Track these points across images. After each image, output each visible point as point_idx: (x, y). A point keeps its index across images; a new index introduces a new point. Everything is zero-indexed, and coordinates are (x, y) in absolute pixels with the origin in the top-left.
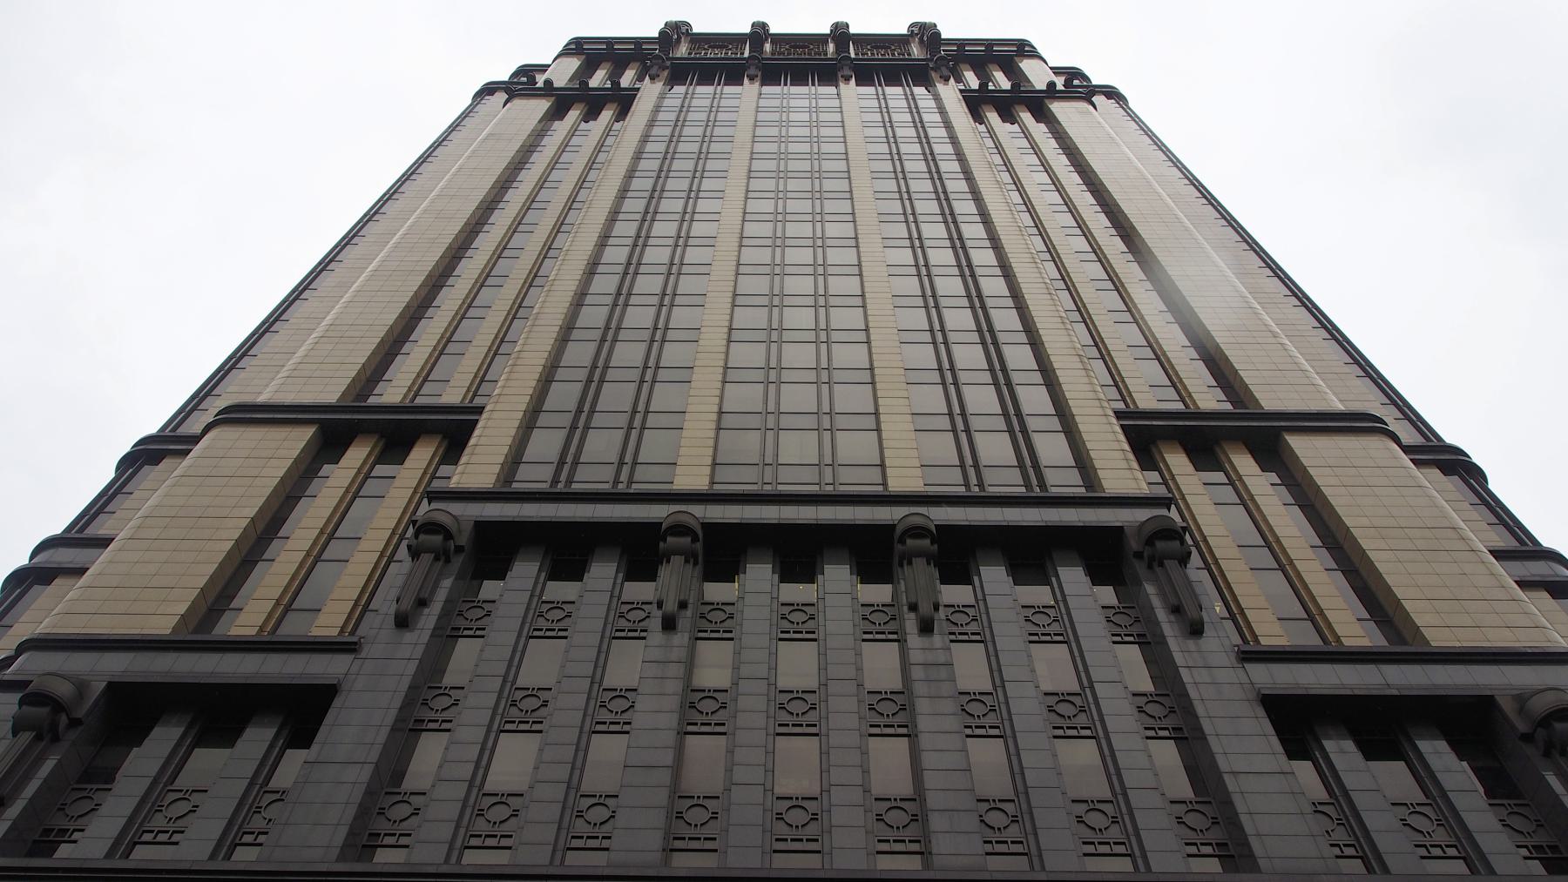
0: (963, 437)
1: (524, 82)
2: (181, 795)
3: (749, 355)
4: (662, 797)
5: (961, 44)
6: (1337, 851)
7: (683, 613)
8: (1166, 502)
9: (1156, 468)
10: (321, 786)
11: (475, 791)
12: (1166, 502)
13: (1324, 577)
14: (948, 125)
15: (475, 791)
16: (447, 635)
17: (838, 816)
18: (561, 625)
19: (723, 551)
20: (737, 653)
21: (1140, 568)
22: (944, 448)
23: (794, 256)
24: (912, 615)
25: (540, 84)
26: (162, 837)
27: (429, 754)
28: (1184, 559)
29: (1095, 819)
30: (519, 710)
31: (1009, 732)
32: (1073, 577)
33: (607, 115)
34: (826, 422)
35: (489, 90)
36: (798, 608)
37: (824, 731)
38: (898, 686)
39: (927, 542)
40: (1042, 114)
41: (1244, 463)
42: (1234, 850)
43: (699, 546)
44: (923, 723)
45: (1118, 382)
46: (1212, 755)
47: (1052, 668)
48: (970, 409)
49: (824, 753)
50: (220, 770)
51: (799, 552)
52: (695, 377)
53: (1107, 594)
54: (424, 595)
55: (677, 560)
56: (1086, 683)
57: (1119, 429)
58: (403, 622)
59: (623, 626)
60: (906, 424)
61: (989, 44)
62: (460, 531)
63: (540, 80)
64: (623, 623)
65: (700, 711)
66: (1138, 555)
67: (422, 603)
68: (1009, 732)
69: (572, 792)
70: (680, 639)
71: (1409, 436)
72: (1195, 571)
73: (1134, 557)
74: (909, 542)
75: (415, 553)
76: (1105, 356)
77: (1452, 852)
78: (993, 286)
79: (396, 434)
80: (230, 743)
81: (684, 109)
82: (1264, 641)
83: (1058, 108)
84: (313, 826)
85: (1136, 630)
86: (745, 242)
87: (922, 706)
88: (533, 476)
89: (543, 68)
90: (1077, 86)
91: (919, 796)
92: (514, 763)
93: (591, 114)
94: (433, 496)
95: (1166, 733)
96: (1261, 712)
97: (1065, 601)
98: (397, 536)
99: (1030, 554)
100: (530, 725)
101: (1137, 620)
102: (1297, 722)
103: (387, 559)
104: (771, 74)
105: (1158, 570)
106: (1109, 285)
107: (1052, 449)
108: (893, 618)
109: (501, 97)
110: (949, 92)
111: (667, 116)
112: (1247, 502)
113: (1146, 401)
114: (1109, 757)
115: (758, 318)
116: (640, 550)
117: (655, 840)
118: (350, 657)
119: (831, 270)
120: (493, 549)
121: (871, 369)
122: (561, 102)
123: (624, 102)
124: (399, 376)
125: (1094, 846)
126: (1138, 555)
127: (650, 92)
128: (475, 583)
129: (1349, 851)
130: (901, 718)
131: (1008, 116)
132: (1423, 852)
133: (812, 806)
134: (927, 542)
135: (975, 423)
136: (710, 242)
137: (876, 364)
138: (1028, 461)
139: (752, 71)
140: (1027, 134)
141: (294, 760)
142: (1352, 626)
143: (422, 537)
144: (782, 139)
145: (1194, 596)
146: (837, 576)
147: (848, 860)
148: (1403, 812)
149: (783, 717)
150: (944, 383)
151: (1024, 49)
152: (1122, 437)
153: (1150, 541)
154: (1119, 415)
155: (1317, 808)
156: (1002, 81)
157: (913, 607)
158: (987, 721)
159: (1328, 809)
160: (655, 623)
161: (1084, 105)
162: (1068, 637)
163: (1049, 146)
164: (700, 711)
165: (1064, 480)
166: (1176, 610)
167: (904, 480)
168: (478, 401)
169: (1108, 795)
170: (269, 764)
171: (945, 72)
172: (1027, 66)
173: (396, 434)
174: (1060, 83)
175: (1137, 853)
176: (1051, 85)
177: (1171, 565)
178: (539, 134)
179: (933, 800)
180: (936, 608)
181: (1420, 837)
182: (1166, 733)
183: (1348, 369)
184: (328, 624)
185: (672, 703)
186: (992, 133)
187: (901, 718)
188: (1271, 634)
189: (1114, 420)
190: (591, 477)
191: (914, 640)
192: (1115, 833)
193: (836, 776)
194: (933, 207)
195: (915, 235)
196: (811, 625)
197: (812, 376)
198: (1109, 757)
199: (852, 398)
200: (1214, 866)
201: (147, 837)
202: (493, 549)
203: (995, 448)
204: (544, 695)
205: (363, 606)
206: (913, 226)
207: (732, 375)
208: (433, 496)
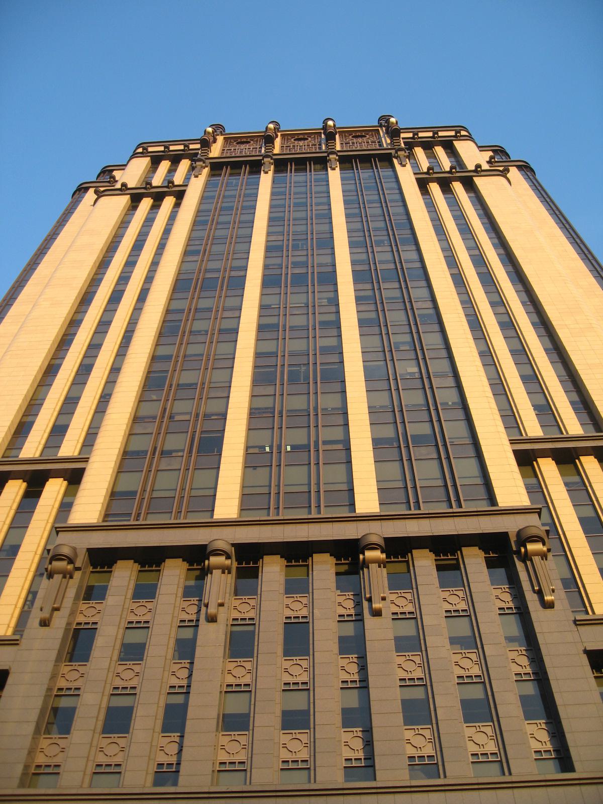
82: (529, 435)
176: (478, 166)
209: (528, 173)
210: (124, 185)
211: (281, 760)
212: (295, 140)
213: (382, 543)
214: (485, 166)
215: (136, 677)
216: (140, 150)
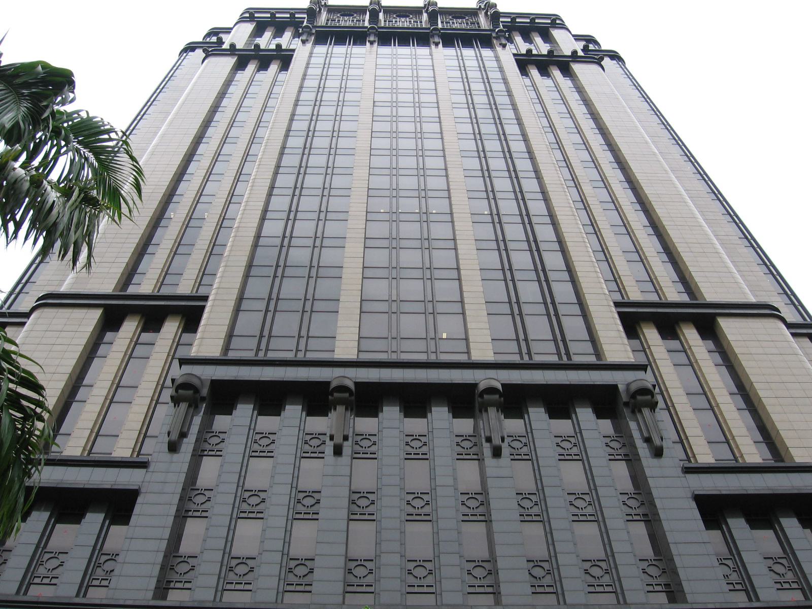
0: (518, 319)
1: (212, 45)
2: (52, 555)
3: (382, 205)
4: (341, 561)
5: (514, 16)
6: (731, 587)
7: (346, 443)
8: (643, 368)
9: (638, 337)
10: (137, 547)
11: (227, 556)
12: (643, 368)
13: (736, 414)
14: (505, 81)
15: (227, 556)
17: (445, 571)
18: (269, 448)
19: (367, 399)
21: (626, 412)
22: (506, 328)
23: (404, 144)
24: (488, 445)
25: (226, 46)
26: (46, 581)
27: (193, 528)
28: (653, 406)
29: (596, 572)
30: (249, 504)
31: (546, 519)
32: (585, 414)
33: (274, 67)
34: (430, 308)
35: (190, 48)
37: (435, 519)
38: (479, 490)
39: (497, 397)
40: (566, 70)
41: (691, 334)
42: (674, 592)
43: (353, 398)
45: (616, 279)
47: (573, 475)
48: (508, 238)
49: (436, 533)
50: (77, 537)
51: (416, 400)
52: (355, 171)
53: (606, 425)
54: (185, 430)
56: (609, 553)
57: (616, 316)
58: (173, 447)
59: (309, 448)
60: (477, 275)
61: (533, 17)
63: (227, 40)
64: (307, 448)
65: (360, 505)
66: (626, 404)
67: (183, 435)
68: (546, 519)
71: (792, 316)
72: (662, 415)
73: (620, 403)
75: (176, 400)
76: (569, 166)
77: (795, 586)
78: (517, 146)
79: (152, 315)
80: (78, 522)
81: (326, 66)
82: (631, 299)
83: (577, 68)
84: (134, 578)
86: (377, 78)
88: (244, 349)
89: (228, 31)
90: (593, 52)
91: (484, 491)
92: (248, 534)
93: (264, 65)
94: (183, 362)
95: (620, 457)
97: (581, 433)
98: (161, 387)
99: (560, 401)
101: (624, 445)
102: (714, 510)
103: (156, 402)
104: (386, 38)
106: (592, 165)
107: (574, 327)
108: (475, 445)
109: (199, 53)
110: (507, 55)
111: (314, 71)
112: (692, 364)
113: (635, 294)
115: (384, 162)
116: (317, 399)
118: (143, 471)
119: (428, 172)
120: (224, 396)
121: (458, 269)
122: (243, 59)
123: (284, 59)
124: (164, 242)
125: (594, 588)
127: (302, 51)
129: (739, 587)
130: (482, 510)
131: (544, 71)
132: (779, 586)
133: (429, 566)
135: (511, 246)
136: (357, 104)
137: (454, 211)
138: (560, 338)
139: (372, 39)
140: (557, 86)
141: (116, 530)
142: (752, 452)
144: (395, 104)
145: (659, 431)
146: (440, 414)
147: (449, 598)
148: (770, 562)
149: (411, 580)
150: (499, 249)
151: (556, 22)
152: (619, 322)
153: (634, 395)
154: (617, 304)
156: (541, 47)
157: (489, 440)
159: (729, 562)
160: (329, 449)
161: (595, 67)
162: (582, 458)
163: (573, 98)
165: (582, 353)
166: (648, 440)
167: (482, 351)
168: (202, 291)
169: (603, 557)
170: (102, 536)
171: (504, 42)
172: (556, 33)
173: (152, 315)
174: (579, 46)
175: (619, 591)
176: (575, 52)
177: (646, 411)
178: (228, 83)
180: (503, 440)
181: (777, 577)
182: (620, 457)
183: (740, 242)
184: (123, 450)
186: (534, 85)
187: (482, 510)
188: (705, 456)
189: (613, 309)
190: (282, 349)
191: (489, 461)
192: (606, 579)
193: (439, 481)
194: (481, 87)
195: (470, 102)
197: (416, 194)
199: (440, 231)
200: (662, 598)
201: (37, 580)
202: (224, 396)
203: (539, 328)
204: (251, 563)
205: (144, 435)
206: (464, 72)
207: (378, 67)
208: (183, 362)
209: (620, 63)
210: (233, 46)
211: (166, 580)
212: (453, 17)
213: (352, 387)
214: (580, 53)
215: (535, 506)
216: (247, 15)
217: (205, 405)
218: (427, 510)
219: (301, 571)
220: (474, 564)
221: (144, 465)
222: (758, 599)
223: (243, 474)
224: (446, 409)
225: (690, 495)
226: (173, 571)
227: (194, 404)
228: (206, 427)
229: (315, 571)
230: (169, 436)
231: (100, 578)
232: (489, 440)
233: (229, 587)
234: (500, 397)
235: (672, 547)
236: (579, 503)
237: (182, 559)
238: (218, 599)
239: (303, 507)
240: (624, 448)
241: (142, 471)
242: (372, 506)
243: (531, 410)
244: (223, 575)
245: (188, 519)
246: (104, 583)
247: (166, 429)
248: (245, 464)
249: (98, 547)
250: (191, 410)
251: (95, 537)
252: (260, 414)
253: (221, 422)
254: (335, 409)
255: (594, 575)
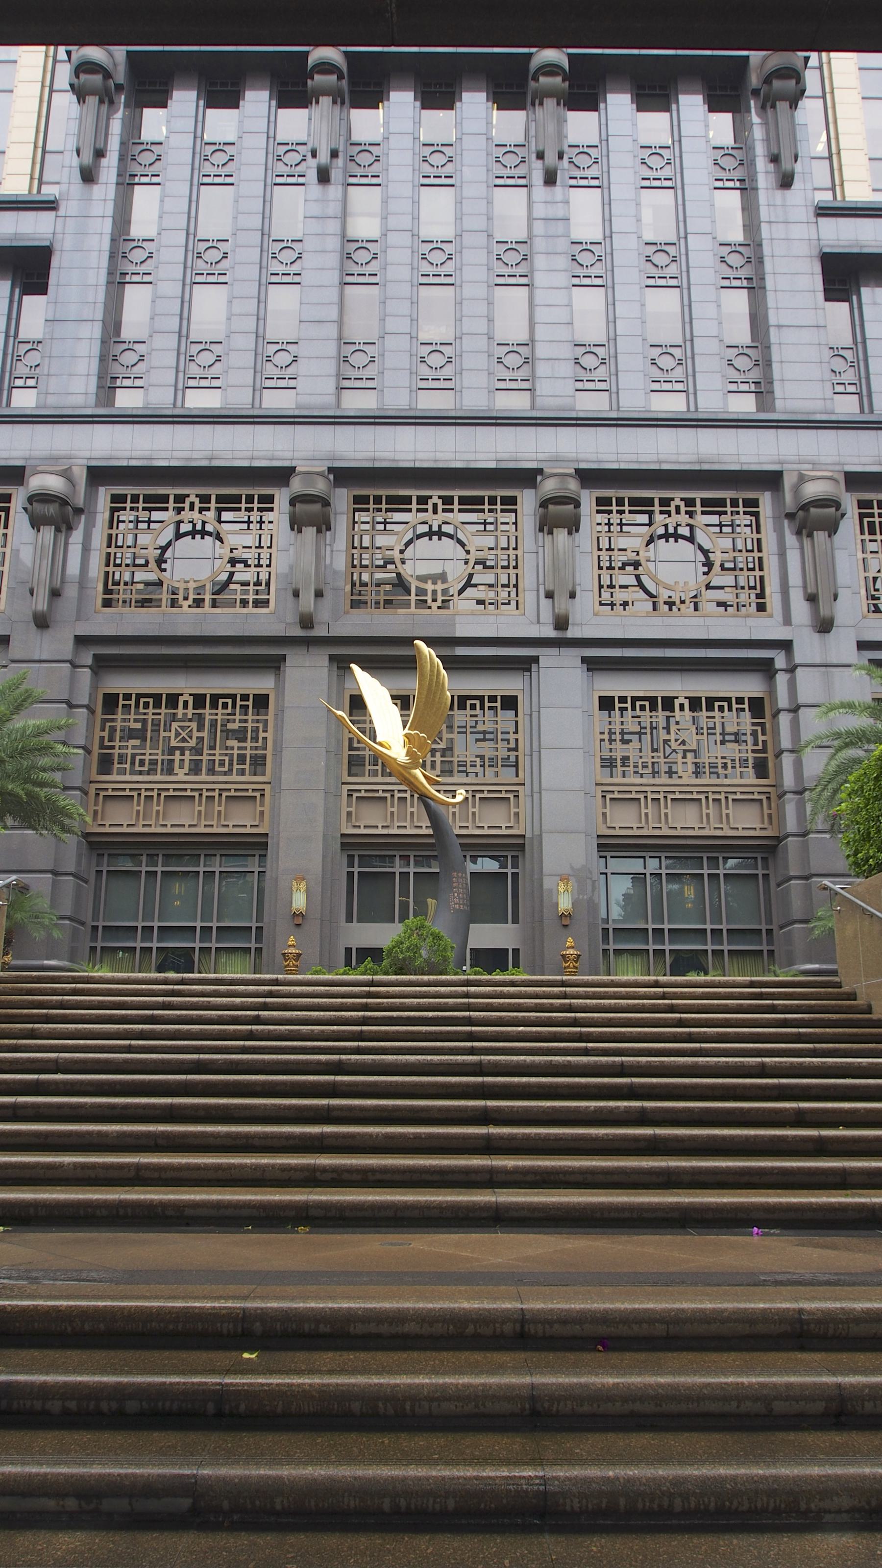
4: (331, 349)
16: (126, 184)
20: (385, 202)
27: (137, 303)
28: (795, 98)
29: (666, 362)
30: (204, 262)
36: (437, 148)
39: (558, 80)
43: (344, 83)
44: (540, 279)
46: (767, 309)
47: (655, 214)
54: (100, 145)
55: (325, 101)
58: (88, 176)
62: (115, 65)
64: (281, 168)
66: (756, 92)
67: (100, 154)
69: (199, 141)
70: (334, 191)
74: (542, 79)
75: (80, 93)
85: (737, 175)
87: (540, 262)
91: (530, 343)
92: (210, 309)
96: (818, 268)
100: (217, 278)
105: (770, 111)
114: (687, 306)
117: (330, 385)
126: (756, 92)
128: (138, 110)
134: (558, 80)
143: (83, 77)
149: (426, 169)
155: (836, 353)
157: (540, 156)
158: (593, 271)
159: (848, 354)
160: (311, 169)
164: (354, 260)
166: (775, 159)
177: (782, 106)
179: (541, 351)
185: (333, 260)
196: (449, 169)
198: (687, 306)
205: (42, 151)
217: (123, 97)
218: (449, 267)
219: (283, 359)
220: (507, 349)
221: (50, 205)
222: (872, 411)
223: (185, 315)
224: (483, 95)
225: (815, 252)
226: (126, 259)
227: (107, 98)
228: (133, 127)
229: (304, 255)
230: (78, 155)
231: (24, 376)
232: (540, 156)
233: (199, 279)
234: (564, 80)
235: (773, 331)
236: (655, 162)
237: (144, 147)
238: (179, 403)
239: (285, 167)
240: (748, 266)
241: (49, 215)
242: (374, 262)
243: (610, 97)
244: (182, 368)
245: (136, 187)
246: (31, 382)
247: (72, 144)
248: (194, 198)
249: (12, 333)
250: (104, 108)
251: (7, 300)
252: (210, 105)
253: (154, 122)
254: (317, 102)
255: (656, 263)
